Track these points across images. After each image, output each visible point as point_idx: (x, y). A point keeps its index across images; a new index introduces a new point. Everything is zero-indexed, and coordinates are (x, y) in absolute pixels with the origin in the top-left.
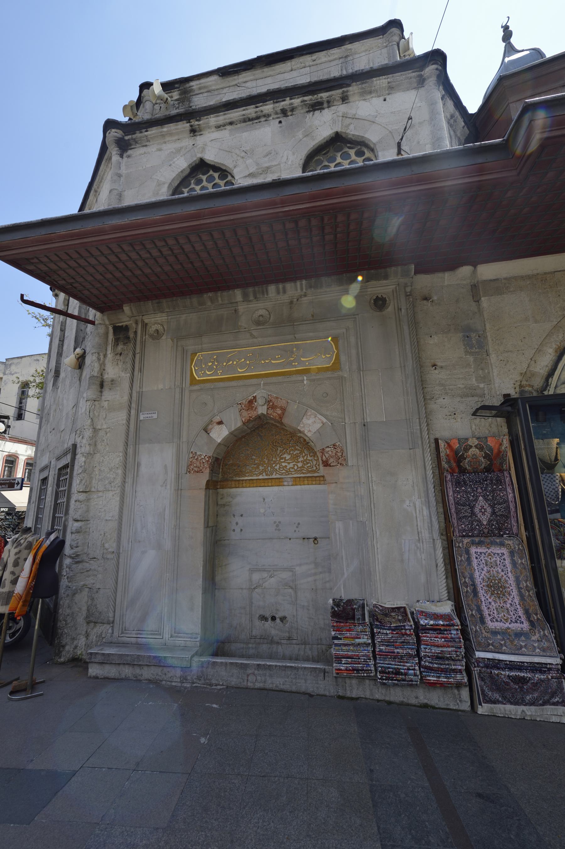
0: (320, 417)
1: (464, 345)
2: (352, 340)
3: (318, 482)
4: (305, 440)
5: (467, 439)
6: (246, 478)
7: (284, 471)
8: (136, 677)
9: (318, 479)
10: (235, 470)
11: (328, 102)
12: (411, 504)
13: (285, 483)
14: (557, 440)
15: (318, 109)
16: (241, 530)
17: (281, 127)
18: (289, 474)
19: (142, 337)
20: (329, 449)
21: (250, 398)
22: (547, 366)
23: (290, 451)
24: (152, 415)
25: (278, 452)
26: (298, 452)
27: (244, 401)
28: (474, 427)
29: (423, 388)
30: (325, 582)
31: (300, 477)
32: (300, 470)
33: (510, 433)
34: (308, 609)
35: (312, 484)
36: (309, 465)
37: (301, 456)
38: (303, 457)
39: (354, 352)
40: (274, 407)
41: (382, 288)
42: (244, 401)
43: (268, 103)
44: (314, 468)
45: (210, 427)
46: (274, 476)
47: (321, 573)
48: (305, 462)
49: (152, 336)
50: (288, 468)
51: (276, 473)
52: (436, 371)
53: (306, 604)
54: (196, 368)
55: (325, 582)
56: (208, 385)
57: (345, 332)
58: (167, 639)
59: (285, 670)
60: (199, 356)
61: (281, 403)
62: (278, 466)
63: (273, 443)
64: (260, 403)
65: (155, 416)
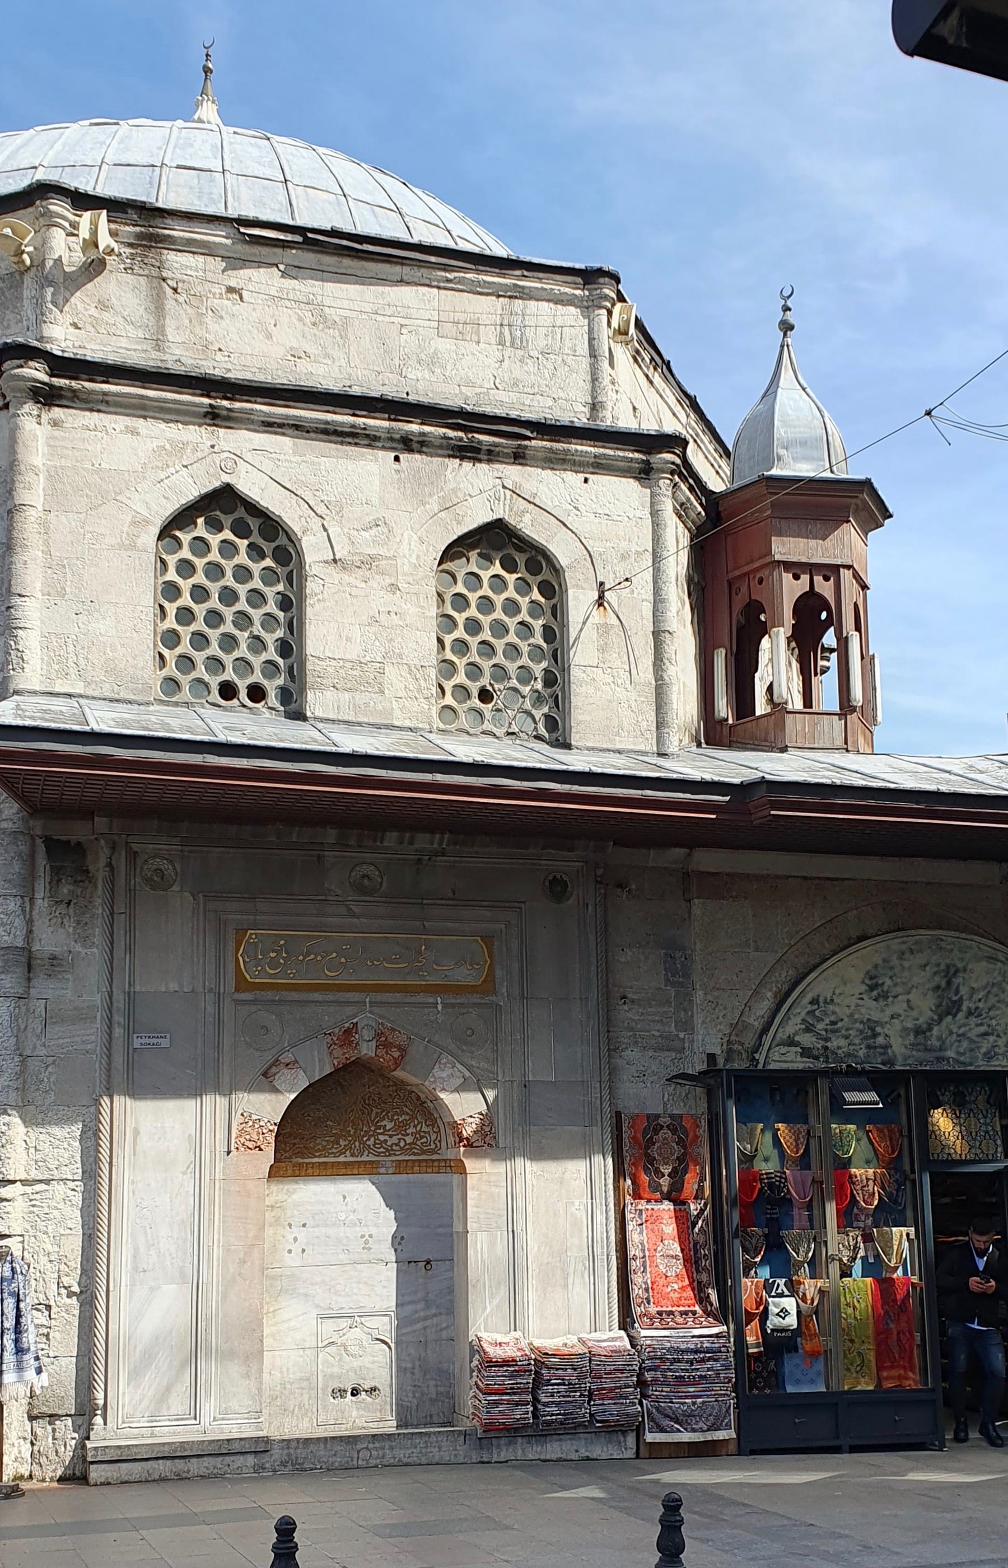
0: (458, 1065)
1: (666, 969)
2: (515, 945)
3: (435, 1170)
4: (418, 1098)
5: (658, 1116)
6: (316, 1160)
7: (382, 1150)
8: (179, 1475)
9: (436, 1164)
10: (295, 1144)
11: (490, 452)
12: (582, 1207)
13: (382, 1170)
14: (761, 1126)
15: (469, 458)
16: (303, 1251)
17: (398, 471)
18: (390, 1155)
19: (128, 881)
20: (472, 1120)
21: (347, 1025)
22: (763, 1017)
23: (393, 1116)
24: (159, 1040)
25: (373, 1116)
26: (407, 1118)
27: (337, 1030)
28: (666, 1096)
29: (609, 1031)
30: (441, 1330)
31: (407, 1161)
32: (409, 1148)
33: (710, 1112)
34: (413, 1373)
35: (427, 1173)
36: (425, 1140)
37: (412, 1124)
38: (415, 1126)
39: (516, 966)
40: (386, 1045)
41: (565, 863)
42: (337, 1030)
43: (377, 415)
44: (433, 1146)
45: (274, 1070)
46: (365, 1158)
47: (435, 1315)
48: (418, 1135)
49: (148, 880)
50: (389, 1143)
51: (369, 1152)
52: (626, 1007)
53: (409, 1365)
54: (247, 960)
55: (441, 1330)
56: (269, 995)
57: (504, 930)
58: (207, 1424)
59: (411, 1439)
60: (250, 937)
61: (401, 1039)
62: (372, 1139)
63: (364, 1100)
64: (366, 1038)
65: (165, 1043)
